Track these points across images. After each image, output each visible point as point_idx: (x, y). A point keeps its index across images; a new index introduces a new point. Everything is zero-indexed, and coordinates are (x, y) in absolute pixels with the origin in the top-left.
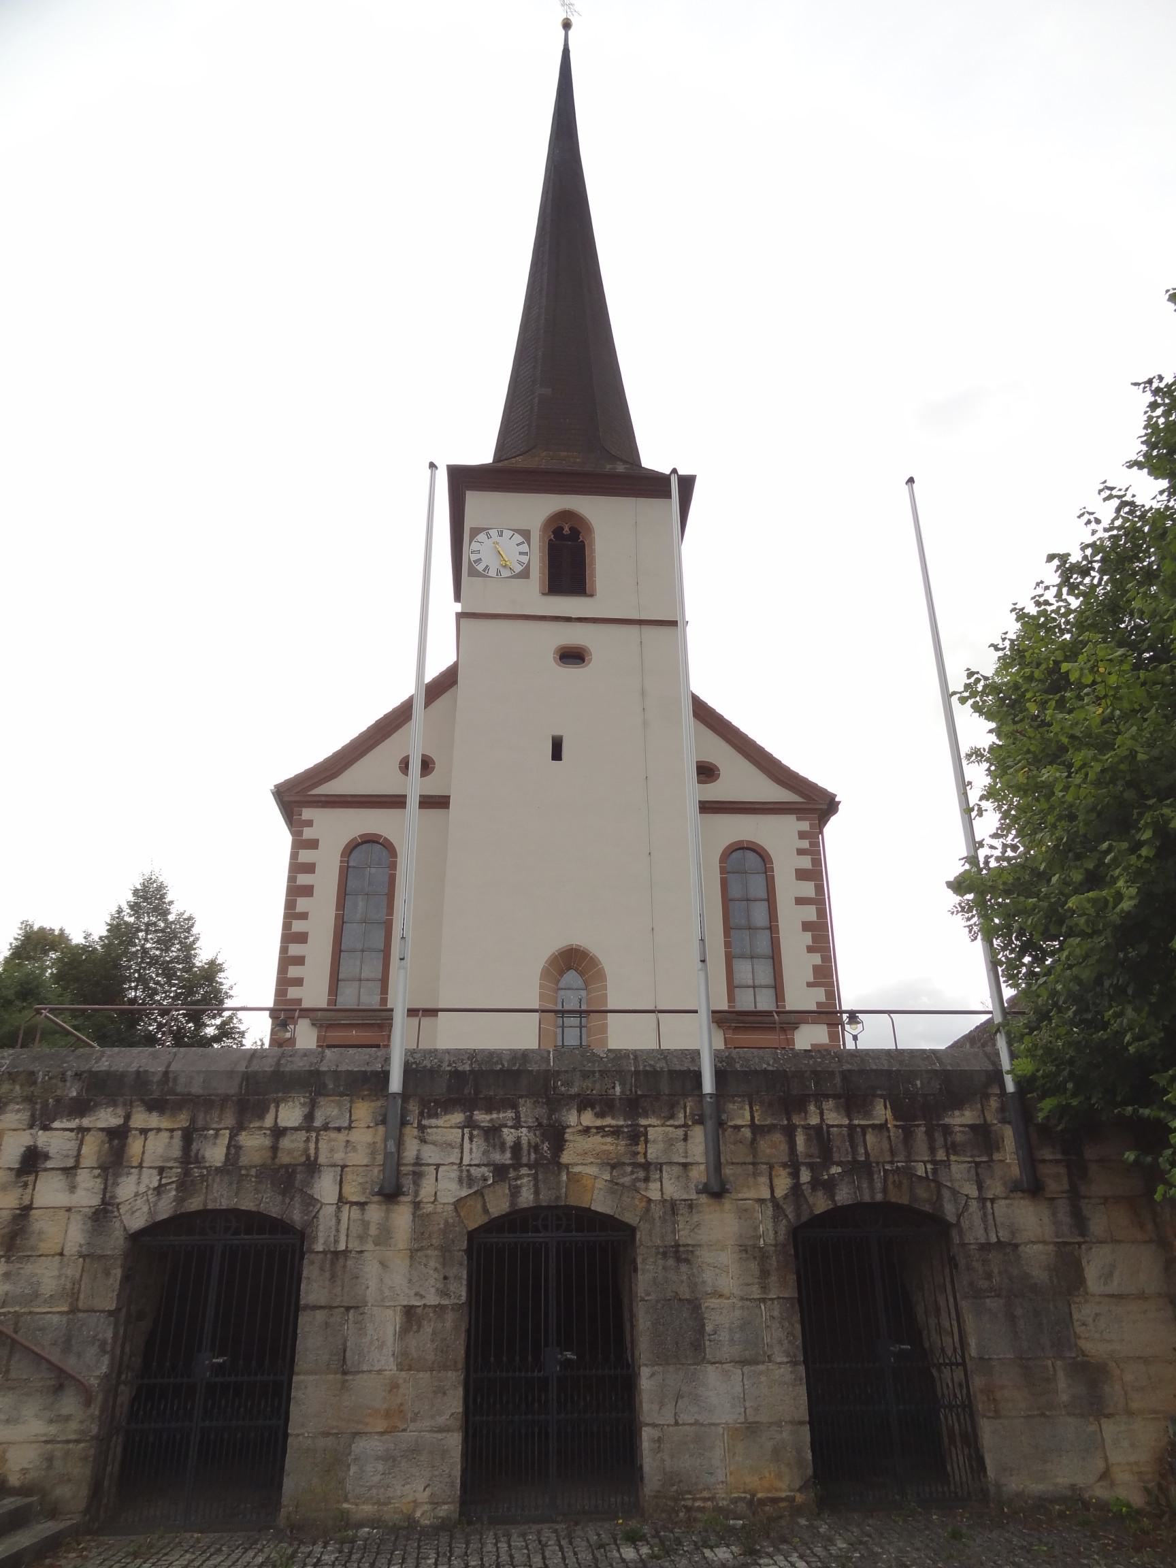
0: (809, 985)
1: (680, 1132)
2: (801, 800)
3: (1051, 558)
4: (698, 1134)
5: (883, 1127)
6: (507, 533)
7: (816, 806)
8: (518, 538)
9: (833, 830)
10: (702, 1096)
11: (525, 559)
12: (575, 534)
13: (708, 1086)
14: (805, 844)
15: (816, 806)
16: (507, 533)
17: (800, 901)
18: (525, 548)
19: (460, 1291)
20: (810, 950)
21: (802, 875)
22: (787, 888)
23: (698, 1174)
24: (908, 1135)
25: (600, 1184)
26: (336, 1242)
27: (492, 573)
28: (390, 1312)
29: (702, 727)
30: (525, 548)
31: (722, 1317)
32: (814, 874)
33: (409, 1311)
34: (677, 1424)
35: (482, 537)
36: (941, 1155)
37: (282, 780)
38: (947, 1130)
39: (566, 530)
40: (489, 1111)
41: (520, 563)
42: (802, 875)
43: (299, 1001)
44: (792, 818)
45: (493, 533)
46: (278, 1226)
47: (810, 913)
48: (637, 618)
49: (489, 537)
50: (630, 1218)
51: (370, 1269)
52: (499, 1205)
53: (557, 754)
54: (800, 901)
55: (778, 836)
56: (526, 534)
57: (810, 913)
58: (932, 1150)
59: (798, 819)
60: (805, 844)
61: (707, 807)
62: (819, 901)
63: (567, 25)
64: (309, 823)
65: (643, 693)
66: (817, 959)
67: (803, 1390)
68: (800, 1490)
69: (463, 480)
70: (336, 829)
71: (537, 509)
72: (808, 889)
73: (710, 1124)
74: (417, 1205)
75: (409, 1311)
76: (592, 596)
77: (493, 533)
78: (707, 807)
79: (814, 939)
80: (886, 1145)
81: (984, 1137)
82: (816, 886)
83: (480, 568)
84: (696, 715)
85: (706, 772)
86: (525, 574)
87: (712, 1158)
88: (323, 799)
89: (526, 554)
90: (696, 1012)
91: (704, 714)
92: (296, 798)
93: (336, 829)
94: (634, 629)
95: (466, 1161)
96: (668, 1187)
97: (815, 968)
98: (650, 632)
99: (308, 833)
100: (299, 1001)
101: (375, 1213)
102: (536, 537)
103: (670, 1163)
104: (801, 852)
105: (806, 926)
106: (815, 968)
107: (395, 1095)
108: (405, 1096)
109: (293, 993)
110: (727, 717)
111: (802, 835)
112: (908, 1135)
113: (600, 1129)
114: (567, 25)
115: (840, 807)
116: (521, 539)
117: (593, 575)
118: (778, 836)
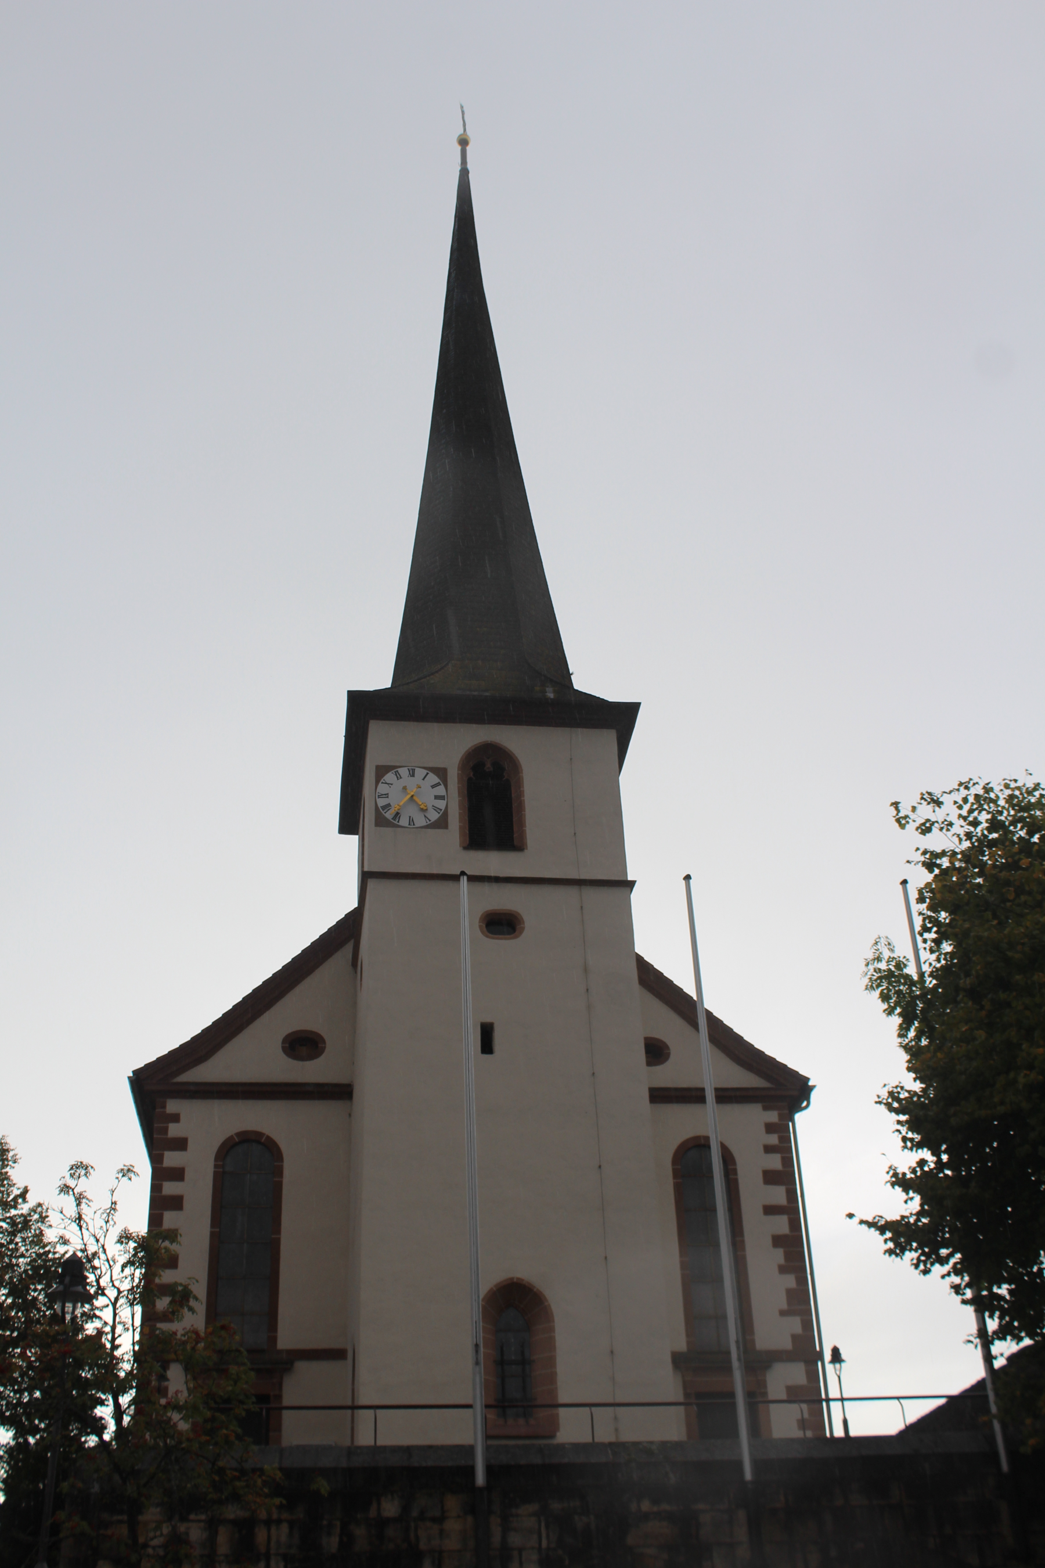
6: (420, 773)
8: (433, 779)
11: (441, 804)
13: (1005, 1466)
14: (773, 1139)
16: (420, 773)
17: (770, 1210)
18: (441, 790)
22: (754, 1194)
27: (404, 821)
35: (390, 777)
37: (140, 1064)
39: (489, 766)
41: (436, 809)
45: (404, 772)
47: (781, 1225)
48: (577, 877)
49: (399, 777)
53: (487, 1046)
54: (770, 1210)
55: (738, 1129)
56: (441, 773)
57: (781, 1225)
59: (765, 1108)
60: (773, 1139)
61: (660, 1096)
63: (463, 142)
64: (176, 1118)
65: (586, 970)
66: (790, 1281)
69: (363, 708)
70: (206, 1126)
71: (454, 743)
72: (778, 1195)
77: (404, 772)
78: (660, 1096)
79: (788, 1256)
83: (389, 815)
85: (656, 1052)
86: (442, 823)
89: (442, 798)
92: (158, 1089)
93: (206, 1126)
94: (572, 892)
97: (789, 1292)
98: (591, 895)
99: (174, 1130)
104: (768, 1149)
105: (778, 1241)
106: (789, 1292)
107: (481, 1489)
108: (489, 1487)
110: (667, 974)
111: (770, 1128)
114: (463, 142)
115: (813, 1095)
116: (436, 780)
117: (522, 824)
118: (738, 1129)
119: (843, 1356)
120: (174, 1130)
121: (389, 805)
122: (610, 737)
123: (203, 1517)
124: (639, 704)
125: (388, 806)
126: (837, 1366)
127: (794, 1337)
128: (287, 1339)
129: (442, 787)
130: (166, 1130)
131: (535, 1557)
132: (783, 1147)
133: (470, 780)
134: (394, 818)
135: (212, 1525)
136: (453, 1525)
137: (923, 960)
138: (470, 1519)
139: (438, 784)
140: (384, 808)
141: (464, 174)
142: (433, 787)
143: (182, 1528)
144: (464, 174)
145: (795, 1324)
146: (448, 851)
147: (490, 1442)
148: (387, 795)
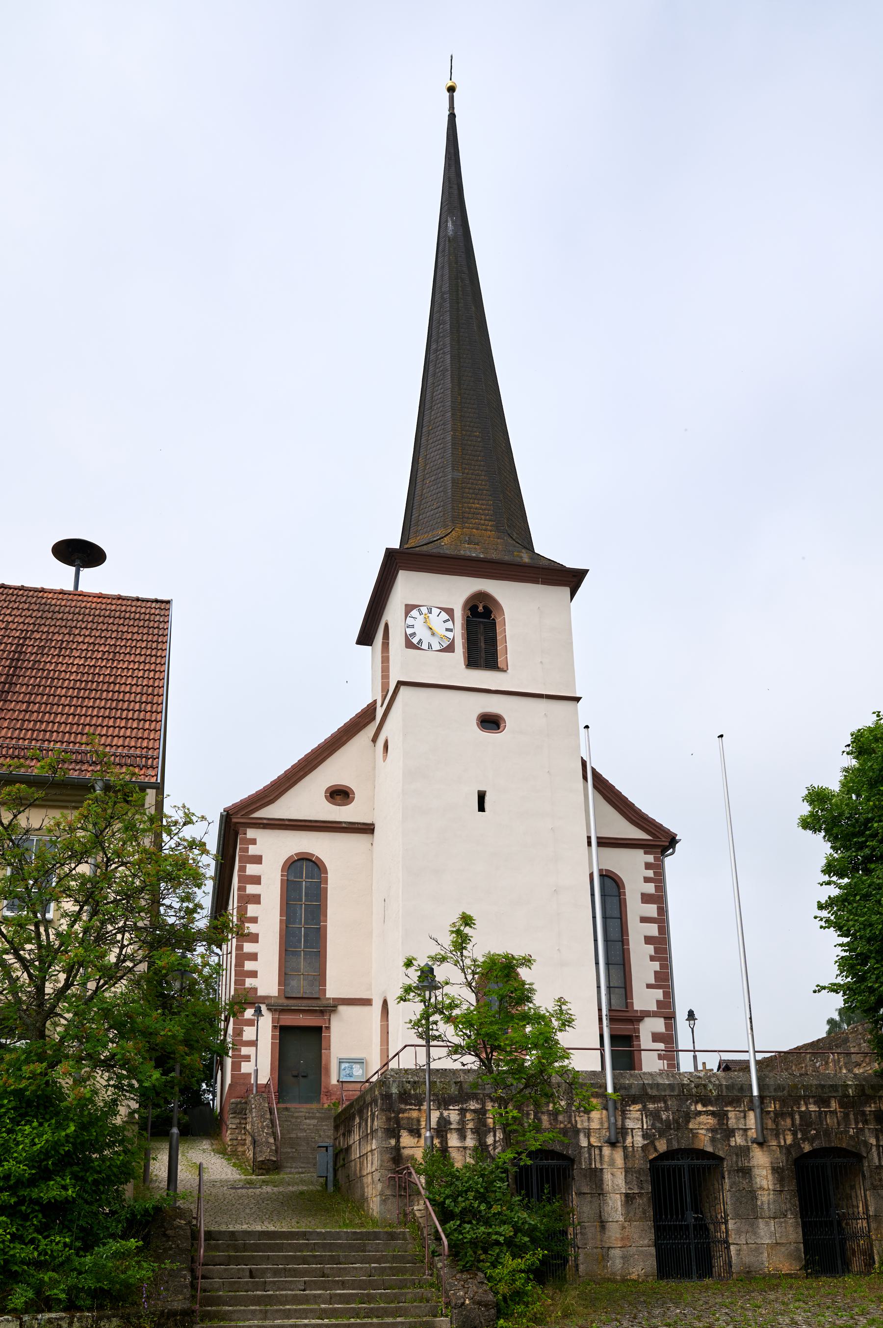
0: (649, 986)
1: (742, 1114)
2: (649, 838)
3: (874, 713)
4: (751, 1115)
5: (834, 1112)
6: (435, 611)
7: (660, 842)
8: (444, 616)
9: (670, 862)
10: (752, 1096)
11: (450, 635)
12: (488, 612)
13: (755, 1092)
14: (650, 873)
15: (660, 842)
16: (435, 611)
17: (644, 920)
18: (449, 625)
19: (649, 1188)
20: (652, 959)
21: (646, 898)
23: (752, 1134)
24: (846, 1115)
25: (707, 1138)
26: (591, 1164)
27: (425, 646)
28: (618, 1196)
30: (449, 625)
31: (765, 1198)
32: (658, 898)
33: (627, 1195)
34: (747, 1244)
35: (414, 613)
36: (860, 1125)
37: (229, 803)
38: (863, 1113)
39: (481, 609)
40: (654, 1103)
42: (646, 898)
43: (256, 989)
44: (641, 851)
45: (424, 610)
50: (721, 1154)
51: (607, 1176)
52: (662, 1146)
53: (481, 797)
54: (644, 920)
55: (632, 867)
56: (450, 612)
57: (653, 930)
58: (857, 1123)
59: (645, 853)
60: (650, 873)
62: (662, 920)
63: (451, 89)
64: (253, 842)
66: (656, 966)
67: (800, 1230)
68: (800, 1269)
71: (457, 591)
72: (651, 910)
73: (758, 1111)
74: (625, 1148)
75: (627, 1195)
76: (504, 671)
77: (424, 610)
80: (835, 1120)
82: (658, 908)
83: (415, 641)
87: (759, 1126)
88: (265, 822)
90: (578, 699)
95: (645, 1127)
96: (738, 1140)
101: (607, 1151)
103: (739, 1129)
105: (648, 940)
109: (249, 982)
111: (648, 866)
113: (706, 1111)
114: (451, 89)
116: (447, 617)
119: (696, 1016)
120: (253, 850)
121: (415, 633)
122: (567, 591)
123: (457, 1108)
125: (414, 634)
126: (692, 1022)
127: (658, 1002)
128: (332, 991)
129: (451, 622)
130: (247, 850)
131: (640, 1133)
132: (658, 878)
133: (468, 617)
134: (418, 643)
135: (463, 1112)
136: (595, 1115)
138: (604, 1112)
139: (448, 620)
141: (452, 117)
142: (445, 622)
143: (446, 1113)
144: (452, 117)
145: (659, 994)
146: (454, 667)
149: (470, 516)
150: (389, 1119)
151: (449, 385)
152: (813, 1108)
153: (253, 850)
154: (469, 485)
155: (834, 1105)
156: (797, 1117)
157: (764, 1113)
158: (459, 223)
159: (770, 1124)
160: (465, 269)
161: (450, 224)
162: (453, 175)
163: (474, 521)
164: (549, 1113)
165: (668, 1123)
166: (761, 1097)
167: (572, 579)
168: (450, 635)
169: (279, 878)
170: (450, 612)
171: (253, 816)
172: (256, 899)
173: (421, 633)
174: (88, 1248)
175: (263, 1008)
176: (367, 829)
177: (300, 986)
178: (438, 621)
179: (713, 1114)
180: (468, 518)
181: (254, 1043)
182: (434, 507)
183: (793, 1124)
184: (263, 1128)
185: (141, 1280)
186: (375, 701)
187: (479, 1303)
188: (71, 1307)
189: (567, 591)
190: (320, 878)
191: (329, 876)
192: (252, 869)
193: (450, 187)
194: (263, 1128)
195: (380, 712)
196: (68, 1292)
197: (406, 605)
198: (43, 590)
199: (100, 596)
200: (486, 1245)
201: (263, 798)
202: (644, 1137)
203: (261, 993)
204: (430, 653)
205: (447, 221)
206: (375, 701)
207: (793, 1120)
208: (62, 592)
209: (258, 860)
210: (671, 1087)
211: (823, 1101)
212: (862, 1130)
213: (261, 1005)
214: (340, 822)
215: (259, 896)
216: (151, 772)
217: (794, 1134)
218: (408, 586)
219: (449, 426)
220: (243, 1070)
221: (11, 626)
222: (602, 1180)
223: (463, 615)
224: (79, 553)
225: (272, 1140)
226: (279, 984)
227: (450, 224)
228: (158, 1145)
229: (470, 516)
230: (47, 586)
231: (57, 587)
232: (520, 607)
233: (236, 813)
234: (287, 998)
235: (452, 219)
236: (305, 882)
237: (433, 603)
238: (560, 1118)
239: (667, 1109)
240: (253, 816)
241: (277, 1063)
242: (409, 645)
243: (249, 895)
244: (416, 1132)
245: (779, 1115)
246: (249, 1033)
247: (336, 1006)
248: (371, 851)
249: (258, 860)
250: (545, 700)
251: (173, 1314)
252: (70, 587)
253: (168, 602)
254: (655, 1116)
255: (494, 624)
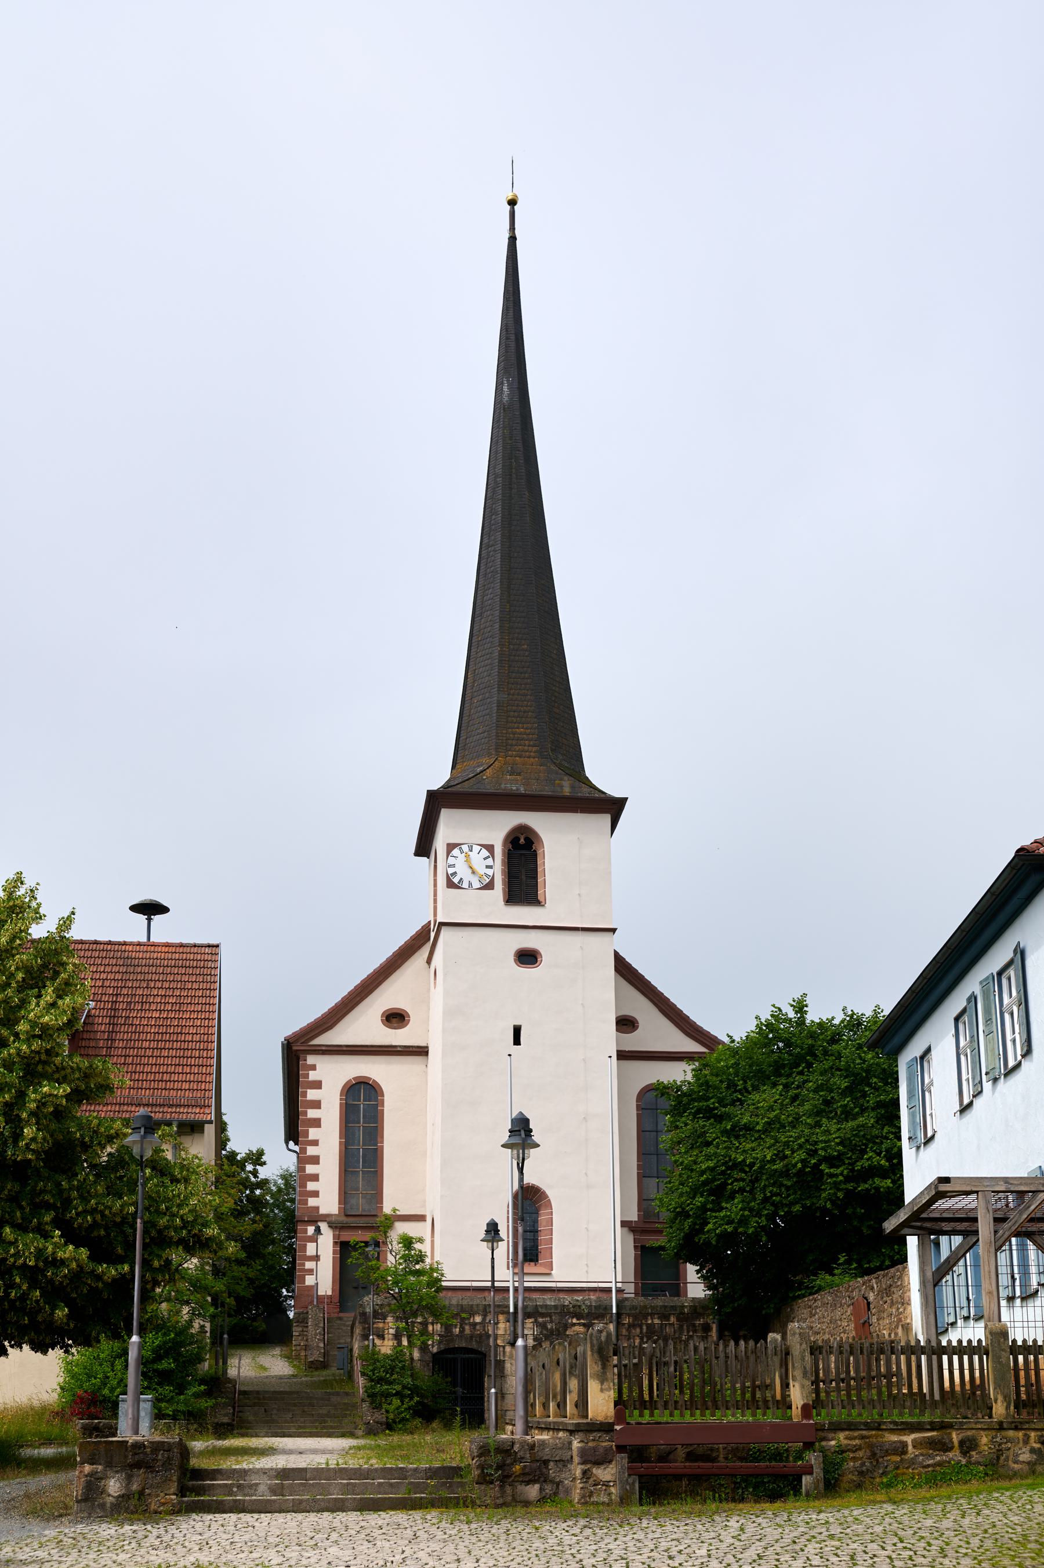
5: (673, 1324)
6: (476, 848)
8: (485, 853)
11: (490, 872)
13: (614, 1311)
16: (476, 848)
18: (490, 862)
24: (681, 1327)
27: (465, 885)
29: (623, 982)
30: (490, 862)
35: (456, 852)
37: (289, 1032)
38: (694, 1325)
39: (522, 841)
43: (317, 1208)
45: (465, 848)
46: (480, 1353)
53: (517, 1031)
56: (490, 848)
58: (688, 1332)
63: (512, 203)
64: (313, 1068)
71: (494, 827)
77: (465, 848)
81: (707, 1328)
83: (456, 880)
84: (617, 970)
85: (626, 1024)
90: (614, 930)
91: (623, 968)
100: (317, 1208)
102: (498, 850)
112: (681, 1327)
114: (512, 203)
116: (488, 854)
120: (313, 1076)
122: (607, 819)
124: (624, 801)
125: (455, 873)
128: (387, 1209)
137: (633, 1216)
140: (452, 874)
141: (513, 240)
144: (513, 240)
146: (493, 906)
147: (527, 1295)
148: (453, 866)
149: (514, 742)
150: (364, 1328)
151: (499, 592)
152: (656, 1321)
153: (313, 1076)
154: (514, 708)
155: (672, 1319)
156: (644, 1327)
157: (619, 1324)
158: (516, 385)
159: (624, 1332)
160: (520, 445)
161: (505, 388)
162: (511, 322)
163: (517, 748)
164: (470, 1324)
165: (552, 1331)
166: (618, 1314)
167: (613, 808)
168: (490, 872)
169: (338, 1102)
170: (490, 848)
171: (312, 1043)
172: (317, 1123)
173: (462, 872)
174: (181, 1393)
175: (323, 1226)
176: (422, 1051)
177: (360, 1205)
178: (478, 857)
179: (584, 1325)
180: (512, 745)
181: (316, 1258)
182: (480, 731)
183: (641, 1332)
184: (316, 1334)
185: (207, 1408)
186: (429, 922)
187: (377, 1422)
188: (174, 1418)
189: (607, 819)
190: (377, 1100)
191: (386, 1098)
192: (312, 1094)
193: (507, 338)
194: (316, 1334)
195: (433, 935)
196: (174, 1411)
197: (448, 845)
198: (125, 944)
199: (167, 945)
200: (387, 1395)
201: (321, 1025)
202: (534, 1340)
203: (322, 1211)
204: (471, 892)
205: (502, 383)
206: (429, 922)
207: (641, 1329)
208: (139, 944)
209: (318, 1085)
210: (556, 1307)
211: (665, 1317)
212: (692, 1337)
213: (320, 1224)
214: (396, 1046)
215: (319, 1120)
216: (207, 1111)
217: (642, 1339)
218: (451, 826)
219: (496, 640)
220: (307, 1283)
221: (107, 983)
222: (504, 1367)
223: (503, 851)
224: (150, 909)
225: (322, 1345)
226: (340, 1203)
227: (505, 388)
228: (233, 1352)
229: (514, 742)
230: (128, 940)
231: (135, 940)
232: (560, 838)
233: (296, 1041)
234: (347, 1216)
235: (508, 381)
236: (363, 1103)
237: (477, 837)
238: (478, 1327)
239: (551, 1322)
240: (312, 1043)
241: (338, 1276)
242: (451, 884)
243: (310, 1120)
244: (382, 1337)
245: (631, 1326)
246: (311, 1249)
247: (393, 1223)
248: (426, 1073)
249: (318, 1085)
250: (580, 933)
251: (223, 1424)
252: (144, 939)
253: (217, 946)
254: (543, 1326)
255: (535, 855)
